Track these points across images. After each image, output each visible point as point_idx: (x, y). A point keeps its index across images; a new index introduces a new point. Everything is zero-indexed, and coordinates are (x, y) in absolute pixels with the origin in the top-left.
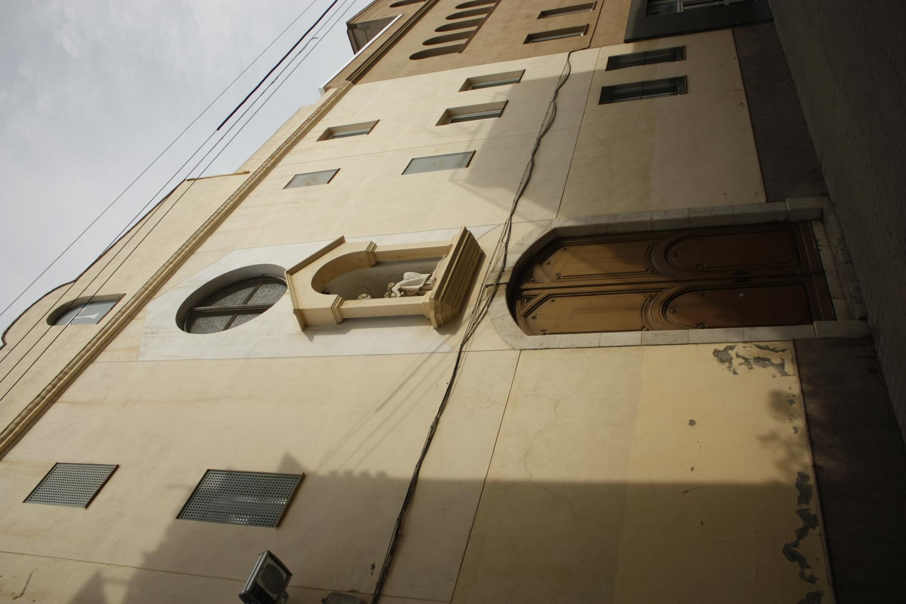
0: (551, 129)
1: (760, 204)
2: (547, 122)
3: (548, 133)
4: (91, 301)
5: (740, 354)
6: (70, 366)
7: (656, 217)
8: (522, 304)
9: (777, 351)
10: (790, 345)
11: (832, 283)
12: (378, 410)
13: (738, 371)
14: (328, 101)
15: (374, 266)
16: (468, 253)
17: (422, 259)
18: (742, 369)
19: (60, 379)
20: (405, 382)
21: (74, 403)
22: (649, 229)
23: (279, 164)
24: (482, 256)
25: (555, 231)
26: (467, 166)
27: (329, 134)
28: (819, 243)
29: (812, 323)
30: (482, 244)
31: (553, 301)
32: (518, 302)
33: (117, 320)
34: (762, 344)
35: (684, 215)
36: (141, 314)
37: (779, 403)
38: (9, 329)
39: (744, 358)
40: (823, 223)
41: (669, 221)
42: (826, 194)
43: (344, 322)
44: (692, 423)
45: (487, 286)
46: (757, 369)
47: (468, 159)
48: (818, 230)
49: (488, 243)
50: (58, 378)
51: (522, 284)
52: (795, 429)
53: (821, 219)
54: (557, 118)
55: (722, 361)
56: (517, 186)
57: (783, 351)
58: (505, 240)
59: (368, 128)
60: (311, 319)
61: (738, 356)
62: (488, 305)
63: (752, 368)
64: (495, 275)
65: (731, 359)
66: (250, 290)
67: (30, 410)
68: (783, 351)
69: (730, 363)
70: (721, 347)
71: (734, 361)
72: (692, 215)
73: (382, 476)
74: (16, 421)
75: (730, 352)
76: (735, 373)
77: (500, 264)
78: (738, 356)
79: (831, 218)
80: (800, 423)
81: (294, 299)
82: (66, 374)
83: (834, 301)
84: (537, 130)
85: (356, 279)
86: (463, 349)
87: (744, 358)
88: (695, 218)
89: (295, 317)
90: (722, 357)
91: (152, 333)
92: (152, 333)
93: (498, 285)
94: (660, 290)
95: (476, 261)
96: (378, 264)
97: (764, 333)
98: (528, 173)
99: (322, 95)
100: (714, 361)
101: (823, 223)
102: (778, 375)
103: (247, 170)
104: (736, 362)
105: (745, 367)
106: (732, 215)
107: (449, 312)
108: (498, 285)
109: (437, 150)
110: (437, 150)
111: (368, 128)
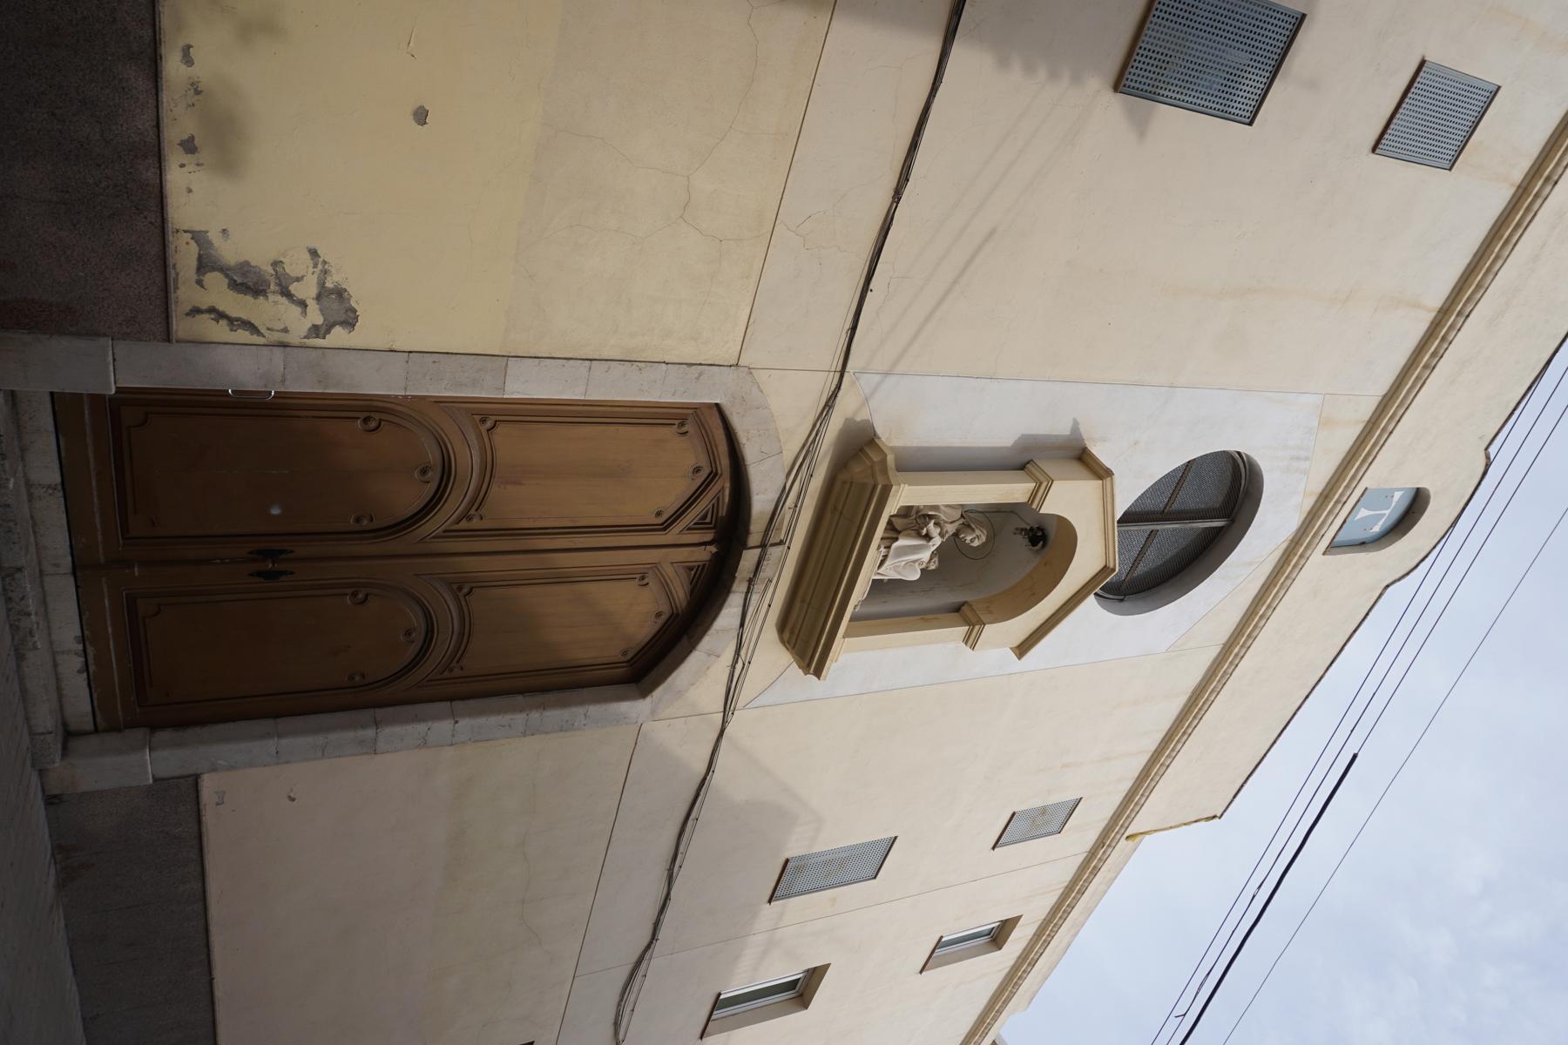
0: (630, 967)
1: (214, 769)
2: (635, 989)
3: (634, 959)
4: (1362, 545)
5: (297, 310)
6: (1421, 382)
7: (443, 727)
8: (715, 508)
9: (212, 310)
10: (182, 327)
11: (57, 541)
12: (992, 232)
13: (307, 256)
14: (990, 1025)
15: (964, 603)
16: (808, 638)
17: (898, 607)
18: (298, 264)
19: (1434, 354)
20: (939, 304)
21: (1416, 305)
22: (458, 705)
23: (1080, 859)
24: (783, 626)
25: (644, 694)
26: (787, 861)
27: (997, 936)
28: (78, 662)
29: (119, 390)
30: (784, 657)
31: (659, 514)
32: (723, 512)
33: (1347, 487)
34: (243, 336)
35: (388, 731)
36: (1309, 503)
37: (223, 142)
38: (1485, 473)
39: (287, 294)
40: (65, 725)
41: (417, 719)
42: (51, 801)
43: (1022, 460)
44: (421, 116)
45: (781, 543)
46: (261, 260)
47: (788, 880)
48: (80, 703)
49: (770, 655)
50: (1438, 355)
51: (715, 555)
52: (188, 59)
53: (69, 735)
54: (616, 999)
55: (340, 293)
56: (707, 810)
57: (196, 311)
58: (739, 666)
59: (942, 952)
60: (1077, 468)
61: (303, 304)
62: (784, 493)
63: (276, 264)
64: (767, 571)
65: (319, 298)
66: (1142, 569)
67: (1479, 286)
68: (196, 311)
69: (322, 284)
70: (338, 336)
71: (314, 291)
72: (369, 733)
73: (1003, 63)
74: (1539, 201)
75: (319, 320)
76: (314, 253)
77: (755, 598)
78: (303, 304)
79: (45, 719)
80: (172, 66)
81: (1108, 499)
82: (1425, 367)
83: (56, 478)
84: (656, 963)
85: (1001, 563)
86: (837, 375)
87: (287, 294)
88: (363, 727)
89: (1106, 461)
90: (339, 308)
91: (1298, 458)
92: (1298, 458)
93: (763, 546)
94: (449, 534)
95: (797, 604)
96: (957, 609)
97: (242, 368)
98: (681, 849)
99: (999, 1036)
100: (359, 298)
101: (65, 725)
102: (214, 236)
103: (1130, 842)
104: (306, 289)
105: (291, 270)
106: (280, 736)
107: (857, 469)
108: (763, 546)
109: (834, 900)
110: (834, 900)
111: (942, 952)
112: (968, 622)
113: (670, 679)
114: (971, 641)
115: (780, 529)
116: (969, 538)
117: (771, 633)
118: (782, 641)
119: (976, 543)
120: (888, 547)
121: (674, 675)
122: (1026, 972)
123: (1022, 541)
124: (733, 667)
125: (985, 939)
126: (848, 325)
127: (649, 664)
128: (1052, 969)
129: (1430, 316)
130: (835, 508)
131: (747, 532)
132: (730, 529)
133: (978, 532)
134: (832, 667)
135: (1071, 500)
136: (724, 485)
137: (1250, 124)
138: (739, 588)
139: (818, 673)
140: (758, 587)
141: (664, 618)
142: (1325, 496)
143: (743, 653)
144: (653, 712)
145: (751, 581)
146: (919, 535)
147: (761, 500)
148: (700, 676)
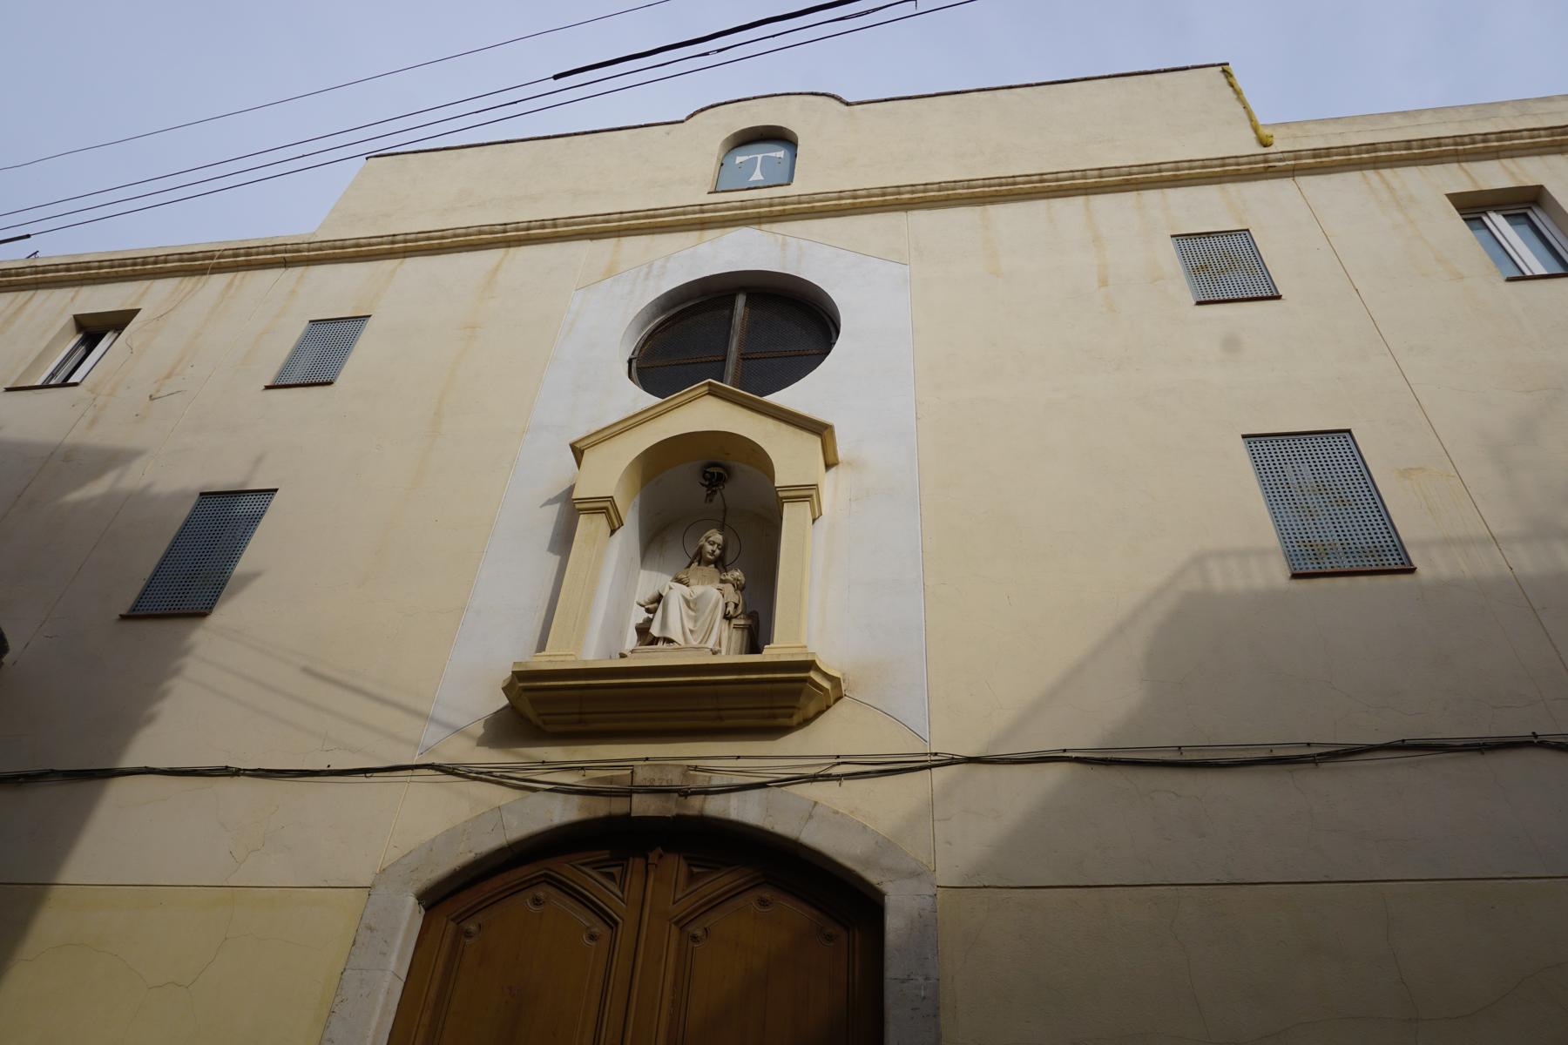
19: (543, 227)
50: (542, 224)
77: (718, 780)
111: (75, 384)
113: (848, 864)
115: (611, 780)
117: (791, 743)
119: (718, 537)
121: (841, 860)
122: (1389, 146)
123: (728, 491)
124: (839, 777)
125: (1538, 217)
126: (361, 778)
127: (838, 897)
128: (1353, 119)
129: (1387, 173)
131: (610, 820)
132: (613, 840)
136: (564, 868)
137: (1349, 431)
138: (695, 805)
140: (701, 780)
141: (767, 894)
142: (703, 225)
143: (812, 771)
144: (915, 874)
145: (685, 793)
147: (560, 812)
148: (842, 821)
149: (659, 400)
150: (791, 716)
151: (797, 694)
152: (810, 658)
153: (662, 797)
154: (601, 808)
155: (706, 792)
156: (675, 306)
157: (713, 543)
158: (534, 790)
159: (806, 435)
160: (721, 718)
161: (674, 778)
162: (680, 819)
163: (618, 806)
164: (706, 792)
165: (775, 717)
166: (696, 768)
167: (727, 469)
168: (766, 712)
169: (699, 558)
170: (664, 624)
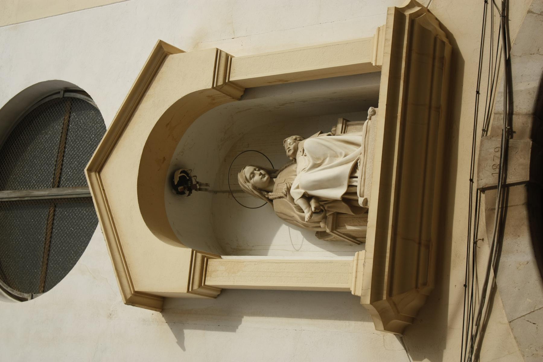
15: (241, 98)
24: (454, 62)
45: (483, 190)
62: (495, 264)
66: (58, 127)
77: (499, 105)
95: (443, 103)
107: (412, 301)
112: (235, 84)
114: (223, 61)
115: (490, 211)
116: (257, 178)
117: (468, 48)
118: (449, 36)
119: (248, 170)
120: (350, 186)
123: (200, 175)
130: (428, 247)
133: (249, 186)
134: (384, 22)
135: (167, 265)
138: (522, 121)
139: (399, 14)
140: (498, 122)
143: (498, 20)
145: (510, 133)
146: (318, 199)
149: (100, 226)
150: (443, 43)
151: (424, 32)
152: (393, 12)
153: (511, 153)
154: (518, 214)
155: (510, 115)
156: (3, 296)
157: (253, 174)
158: (494, 288)
159: (164, 69)
160: (438, 108)
161: (494, 146)
162: (536, 135)
163: (518, 197)
164: (510, 115)
165: (442, 58)
166: (485, 131)
167: (177, 167)
168: (437, 64)
169: (263, 190)
170: (332, 182)
